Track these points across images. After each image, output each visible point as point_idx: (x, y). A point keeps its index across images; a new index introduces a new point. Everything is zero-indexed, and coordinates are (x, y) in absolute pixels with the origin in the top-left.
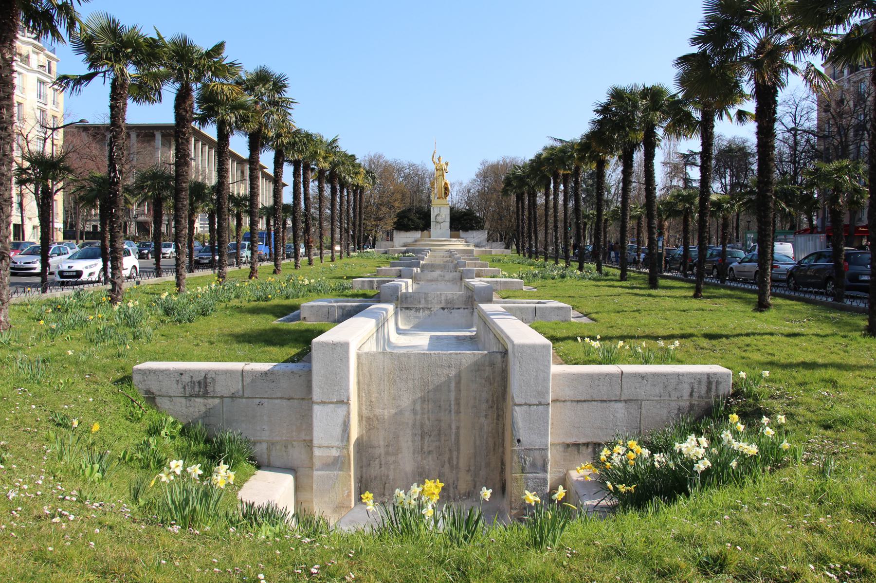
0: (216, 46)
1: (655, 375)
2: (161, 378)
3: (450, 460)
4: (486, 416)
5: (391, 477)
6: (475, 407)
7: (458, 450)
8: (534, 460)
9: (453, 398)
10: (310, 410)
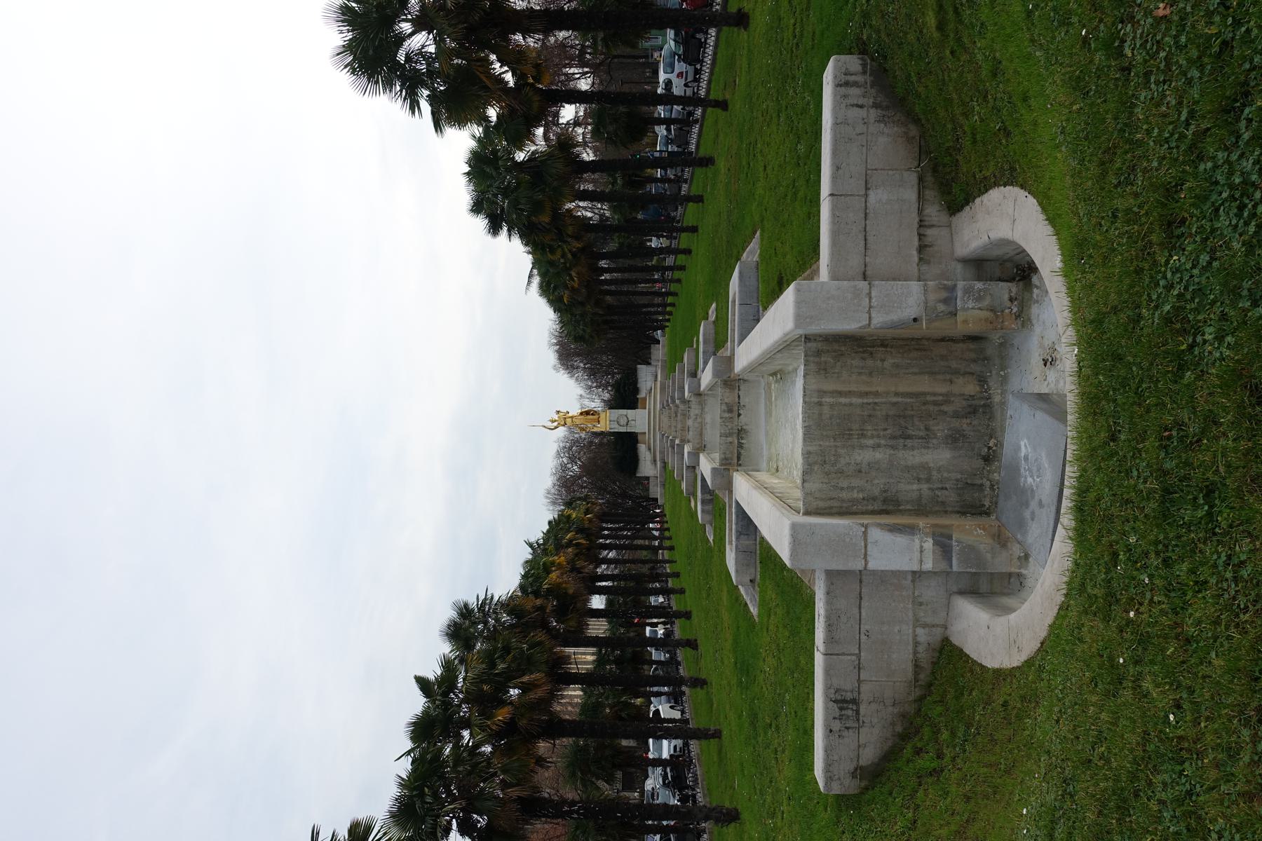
0: (422, 689)
1: (835, 152)
2: (836, 758)
3: (935, 403)
4: (882, 360)
5: (959, 476)
6: (870, 374)
7: (924, 394)
8: (940, 301)
9: (860, 401)
10: (874, 572)
